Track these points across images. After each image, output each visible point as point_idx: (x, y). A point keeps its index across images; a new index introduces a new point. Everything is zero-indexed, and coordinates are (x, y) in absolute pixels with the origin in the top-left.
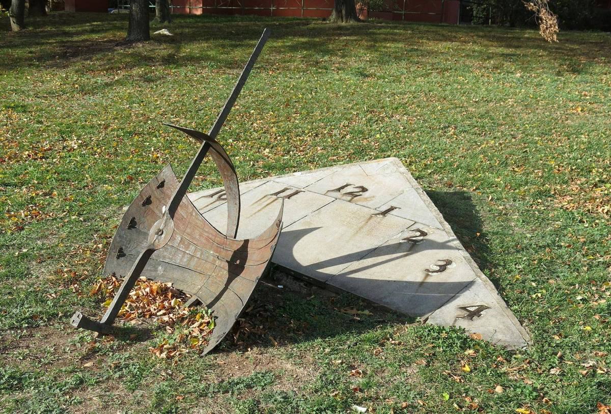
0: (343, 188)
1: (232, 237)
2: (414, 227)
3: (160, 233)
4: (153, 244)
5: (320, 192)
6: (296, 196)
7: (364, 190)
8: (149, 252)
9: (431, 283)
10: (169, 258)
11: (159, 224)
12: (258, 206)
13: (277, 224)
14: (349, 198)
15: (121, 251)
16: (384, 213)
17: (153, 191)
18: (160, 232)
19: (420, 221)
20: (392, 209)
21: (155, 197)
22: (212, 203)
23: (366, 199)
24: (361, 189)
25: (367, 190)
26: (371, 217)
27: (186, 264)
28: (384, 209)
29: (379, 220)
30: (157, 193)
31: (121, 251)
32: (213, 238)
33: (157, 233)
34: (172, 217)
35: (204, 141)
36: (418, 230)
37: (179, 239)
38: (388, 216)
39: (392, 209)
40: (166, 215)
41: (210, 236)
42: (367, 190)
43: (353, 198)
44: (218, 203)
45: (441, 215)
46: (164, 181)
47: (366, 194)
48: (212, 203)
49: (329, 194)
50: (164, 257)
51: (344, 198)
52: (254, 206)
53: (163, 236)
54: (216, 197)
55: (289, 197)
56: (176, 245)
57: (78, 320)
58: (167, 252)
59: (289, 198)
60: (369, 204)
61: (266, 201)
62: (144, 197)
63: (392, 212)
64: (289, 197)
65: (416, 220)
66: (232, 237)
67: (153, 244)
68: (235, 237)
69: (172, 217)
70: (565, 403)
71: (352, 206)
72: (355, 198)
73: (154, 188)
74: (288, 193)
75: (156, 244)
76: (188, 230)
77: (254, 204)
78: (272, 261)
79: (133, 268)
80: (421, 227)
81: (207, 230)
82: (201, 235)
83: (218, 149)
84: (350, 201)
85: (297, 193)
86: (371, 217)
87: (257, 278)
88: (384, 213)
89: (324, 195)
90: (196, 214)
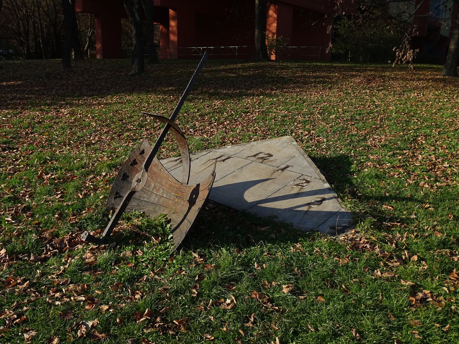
0: (257, 154)
1: (185, 184)
2: (302, 178)
3: (140, 181)
4: (135, 188)
5: (243, 158)
6: (228, 160)
7: (270, 155)
8: (133, 193)
9: (313, 211)
10: (147, 198)
11: (138, 176)
12: (204, 166)
13: (212, 174)
14: (261, 161)
15: (117, 193)
16: (283, 170)
17: (137, 157)
18: (139, 181)
19: (305, 174)
20: (288, 167)
21: (138, 160)
22: (176, 165)
23: (271, 161)
24: (268, 155)
25: (272, 156)
26: (274, 172)
27: (157, 201)
28: (283, 166)
29: (279, 174)
30: (139, 157)
31: (117, 193)
32: (174, 185)
33: (137, 181)
34: (147, 171)
35: (167, 123)
36: (304, 179)
37: (153, 186)
38: (285, 171)
39: (288, 167)
40: (142, 169)
41: (172, 184)
42: (272, 156)
43: (263, 161)
44: (179, 165)
45: (319, 170)
46: (144, 150)
47: (271, 158)
48: (176, 165)
49: (249, 158)
50: (144, 198)
51: (258, 160)
52: (202, 166)
53: (141, 183)
54: (178, 161)
55: (224, 161)
56: (151, 190)
57: (86, 237)
58: (145, 194)
59: (224, 161)
60: (274, 164)
61: (209, 163)
62: (131, 160)
63: (288, 169)
64: (224, 161)
65: (303, 173)
66: (185, 184)
67: (135, 188)
68: (187, 184)
69: (147, 171)
70: (424, 263)
71: (263, 165)
72: (265, 160)
73: (138, 154)
74: (223, 158)
75: (136, 188)
76: (159, 180)
77: (202, 165)
78: (209, 198)
79: (122, 203)
80: (306, 178)
81: (170, 180)
82: (166, 183)
83: (175, 127)
84: (261, 162)
85: (229, 158)
86: (274, 172)
87: (199, 208)
88: (283, 170)
89: (246, 159)
90: (164, 170)
